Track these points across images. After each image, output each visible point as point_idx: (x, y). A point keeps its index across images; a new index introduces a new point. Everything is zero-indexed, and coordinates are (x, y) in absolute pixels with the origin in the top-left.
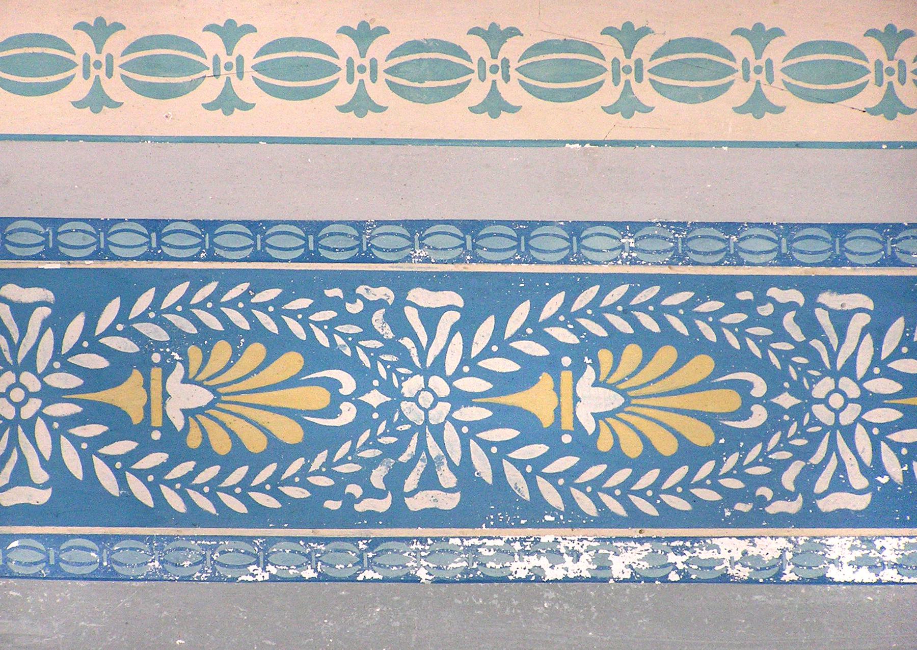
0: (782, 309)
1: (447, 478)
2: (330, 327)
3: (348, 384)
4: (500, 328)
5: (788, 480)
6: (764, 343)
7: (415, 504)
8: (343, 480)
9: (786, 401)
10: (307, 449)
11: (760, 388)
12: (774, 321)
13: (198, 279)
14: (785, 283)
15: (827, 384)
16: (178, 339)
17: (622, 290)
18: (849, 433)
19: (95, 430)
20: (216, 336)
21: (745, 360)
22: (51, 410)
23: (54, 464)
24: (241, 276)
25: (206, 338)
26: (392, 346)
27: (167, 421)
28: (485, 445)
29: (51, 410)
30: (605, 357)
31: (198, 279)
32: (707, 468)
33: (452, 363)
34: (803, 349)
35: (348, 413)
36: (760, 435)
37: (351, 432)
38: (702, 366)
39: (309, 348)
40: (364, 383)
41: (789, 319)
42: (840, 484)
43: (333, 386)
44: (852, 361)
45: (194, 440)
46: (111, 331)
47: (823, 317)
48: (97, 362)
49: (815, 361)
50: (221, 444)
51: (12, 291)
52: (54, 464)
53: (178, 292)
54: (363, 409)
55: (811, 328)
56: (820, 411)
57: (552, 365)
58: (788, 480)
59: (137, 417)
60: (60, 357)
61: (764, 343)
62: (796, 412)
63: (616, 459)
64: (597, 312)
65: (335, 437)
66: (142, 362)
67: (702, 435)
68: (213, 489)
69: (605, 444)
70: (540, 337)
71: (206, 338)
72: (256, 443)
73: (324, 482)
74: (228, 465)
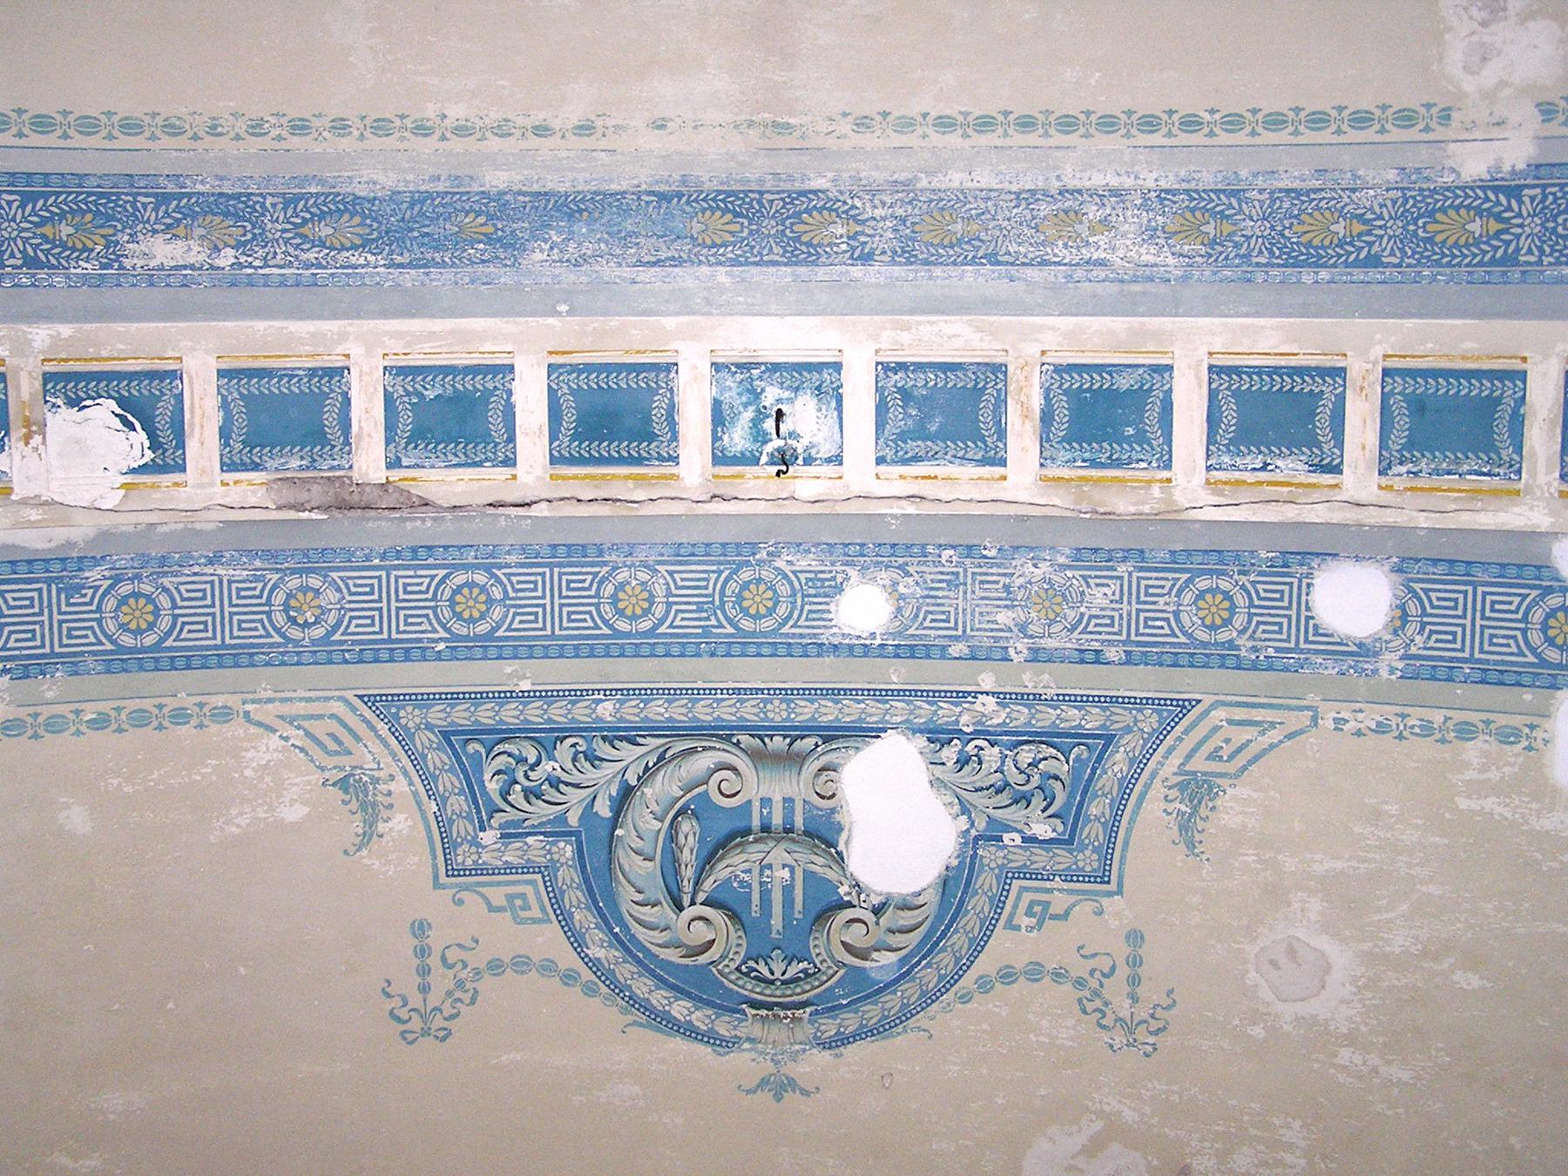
1: (1527, 200)
3: (249, 227)
4: (1506, 251)
5: (1411, 202)
7: (1538, 190)
10: (1434, 211)
11: (249, 227)
15: (1535, 231)
16: (1477, 245)
17: (1475, 261)
18: (15, 240)
19: (1506, 215)
22: (22, 235)
25: (1467, 245)
27: (1481, 218)
28: (31, 245)
29: (22, 235)
30: (1336, 241)
34: (133, 215)
35: (1420, 223)
36: (1421, 216)
39: (802, 243)
41: (1410, 253)
42: (1532, 199)
44: (148, 219)
45: (70, 244)
46: (41, 210)
47: (1398, 255)
48: (169, 221)
49: (1539, 238)
50: (1463, 212)
51: (5, 196)
52: (1520, 202)
54: (1555, 221)
55: (1542, 252)
56: (1539, 222)
58: (1411, 202)
59: (1491, 219)
60: (1518, 237)
62: (1408, 223)
64: (65, 202)
66: (51, 219)
67: (1439, 216)
68: (1467, 196)
70: (47, 210)
71: (1467, 245)
72: (1452, 213)
73: (1429, 200)
74: (1461, 205)
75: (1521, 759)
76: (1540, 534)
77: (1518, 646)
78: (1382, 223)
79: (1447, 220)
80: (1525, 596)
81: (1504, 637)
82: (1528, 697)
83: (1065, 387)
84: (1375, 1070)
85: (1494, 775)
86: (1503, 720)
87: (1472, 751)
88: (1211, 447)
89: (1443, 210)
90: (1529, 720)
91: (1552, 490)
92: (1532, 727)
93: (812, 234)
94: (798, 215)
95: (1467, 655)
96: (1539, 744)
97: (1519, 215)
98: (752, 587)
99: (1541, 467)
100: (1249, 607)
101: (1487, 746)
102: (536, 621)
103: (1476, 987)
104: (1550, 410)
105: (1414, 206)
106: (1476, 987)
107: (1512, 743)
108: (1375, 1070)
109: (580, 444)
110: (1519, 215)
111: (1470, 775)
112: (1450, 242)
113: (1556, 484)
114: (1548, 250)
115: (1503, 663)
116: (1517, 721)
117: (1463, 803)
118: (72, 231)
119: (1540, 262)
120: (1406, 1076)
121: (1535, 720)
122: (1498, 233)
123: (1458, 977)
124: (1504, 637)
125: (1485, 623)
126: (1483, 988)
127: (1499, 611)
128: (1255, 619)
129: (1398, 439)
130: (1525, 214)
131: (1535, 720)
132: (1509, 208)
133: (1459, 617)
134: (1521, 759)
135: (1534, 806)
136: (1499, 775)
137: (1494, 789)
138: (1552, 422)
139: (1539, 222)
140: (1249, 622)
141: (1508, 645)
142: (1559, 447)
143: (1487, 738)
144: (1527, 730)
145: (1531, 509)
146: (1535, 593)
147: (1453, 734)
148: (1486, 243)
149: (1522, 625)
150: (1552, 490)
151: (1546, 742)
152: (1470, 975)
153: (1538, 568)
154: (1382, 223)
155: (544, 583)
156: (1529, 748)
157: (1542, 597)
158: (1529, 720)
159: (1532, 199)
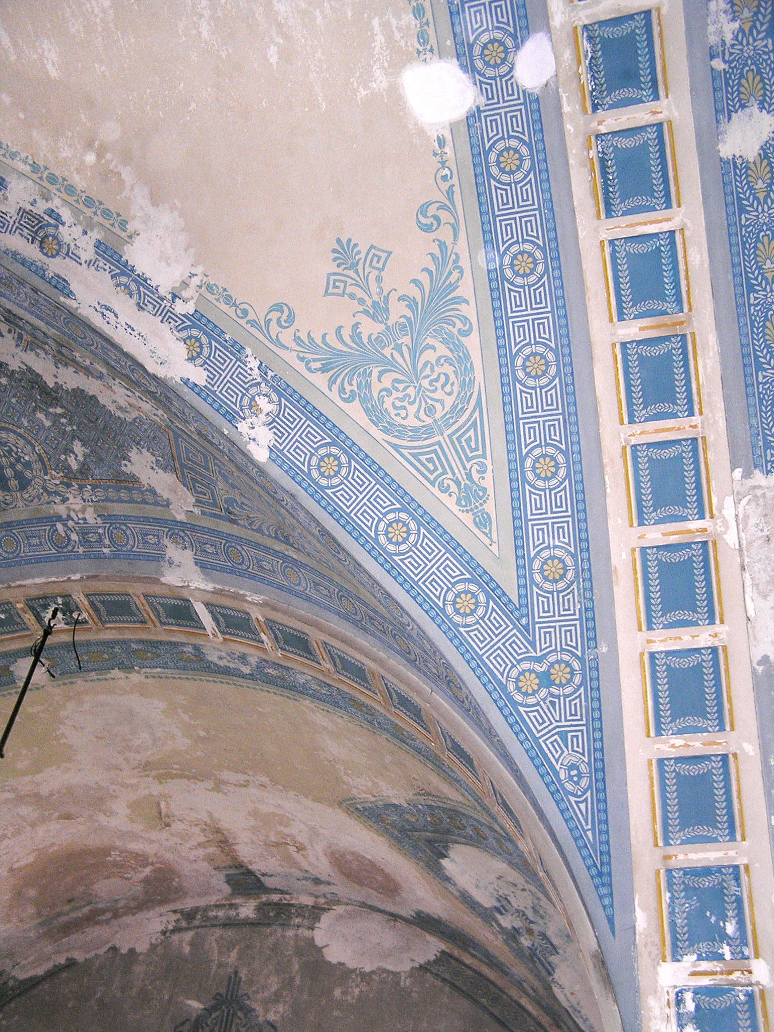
0: (755, 310)
2: (751, 239)
3: (762, 233)
4: (756, 285)
6: (737, 69)
8: (767, 65)
9: (765, 228)
11: (762, 233)
12: (766, 390)
13: (754, 344)
14: (767, 467)
20: (764, 324)
21: (766, 316)
23: (762, 39)
24: (752, 329)
26: (738, 61)
31: (754, 344)
32: (765, 75)
33: (765, 293)
35: (753, 67)
37: (757, 66)
38: (743, 81)
39: (740, 78)
40: (746, 65)
42: (766, 46)
43: (748, 71)
48: (755, 202)
52: (762, 39)
53: (730, 102)
57: (754, 194)
61: (737, 69)
62: (752, 59)
63: (764, 95)
65: (759, 69)
67: (758, 78)
69: (755, 9)
71: (756, 262)
72: (761, 85)
73: (768, 68)
75: (411, 49)
76: (548, 24)
77: (493, 137)
78: (766, 210)
79: (756, 82)
80: (508, 24)
81: (481, 19)
82: (449, 43)
83: (704, 664)
84: (201, 16)
85: (397, 35)
86: (431, 31)
87: (408, 18)
88: (597, 26)
89: (762, 80)
90: (435, 47)
91: (576, 22)
92: (431, 50)
93: (746, 85)
94: (759, 72)
95: (521, 416)
96: (423, 57)
97: (755, 40)
98: (487, 59)
99: (589, 11)
100: (504, 139)
101: (413, 26)
102: (540, 725)
103: (271, 61)
104: (625, 7)
105: (763, 60)
106: (271, 61)
107: (419, 42)
108: (201, 16)
109: (663, 717)
110: (755, 40)
111: (394, 22)
112: (767, 331)
113: (581, 23)
114: (733, 65)
115: (466, 22)
116: (433, 41)
117: (376, 22)
118: (760, 181)
119: (759, 383)
120: (205, 35)
121: (436, 51)
122: (758, 199)
123: (273, 49)
124: (481, 19)
125: (541, 423)
126: (271, 65)
127: (549, 430)
128: (543, 493)
129: (608, 32)
130: (755, 44)
131: (436, 51)
132: (759, 33)
133: (542, 407)
134: (411, 49)
135: (386, 64)
136: (398, 39)
137: (389, 38)
138: (619, 10)
139: (751, 54)
140: (540, 490)
141: (477, 23)
142: (603, 19)
143: (418, 26)
144: (429, 47)
145: (563, 13)
146: (512, 30)
147: (415, 4)
148: (768, 352)
149: (538, 389)
150: (576, 22)
151: (425, 60)
152: (276, 56)
153: (527, 27)
154: (766, 210)
155: (541, 514)
156: (419, 52)
157: (511, 35)
158: (435, 47)
159: (766, 46)
